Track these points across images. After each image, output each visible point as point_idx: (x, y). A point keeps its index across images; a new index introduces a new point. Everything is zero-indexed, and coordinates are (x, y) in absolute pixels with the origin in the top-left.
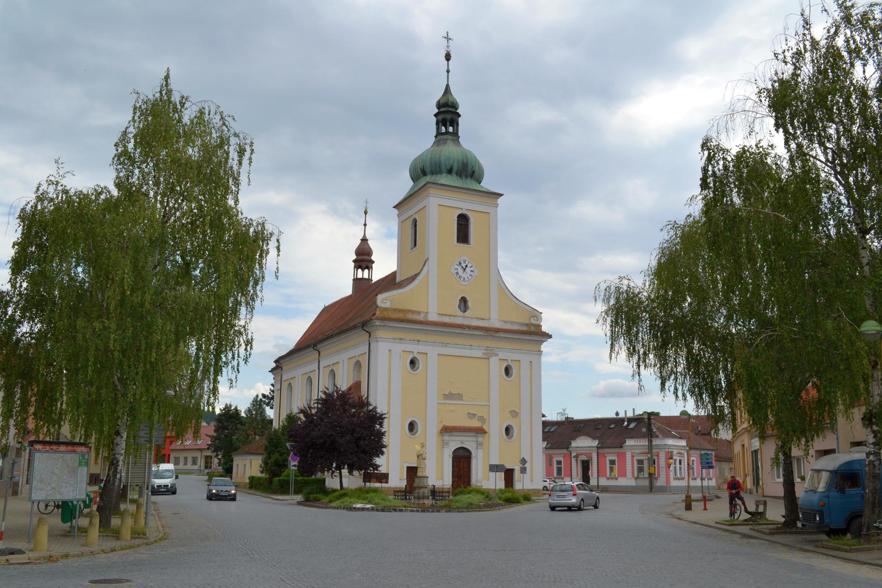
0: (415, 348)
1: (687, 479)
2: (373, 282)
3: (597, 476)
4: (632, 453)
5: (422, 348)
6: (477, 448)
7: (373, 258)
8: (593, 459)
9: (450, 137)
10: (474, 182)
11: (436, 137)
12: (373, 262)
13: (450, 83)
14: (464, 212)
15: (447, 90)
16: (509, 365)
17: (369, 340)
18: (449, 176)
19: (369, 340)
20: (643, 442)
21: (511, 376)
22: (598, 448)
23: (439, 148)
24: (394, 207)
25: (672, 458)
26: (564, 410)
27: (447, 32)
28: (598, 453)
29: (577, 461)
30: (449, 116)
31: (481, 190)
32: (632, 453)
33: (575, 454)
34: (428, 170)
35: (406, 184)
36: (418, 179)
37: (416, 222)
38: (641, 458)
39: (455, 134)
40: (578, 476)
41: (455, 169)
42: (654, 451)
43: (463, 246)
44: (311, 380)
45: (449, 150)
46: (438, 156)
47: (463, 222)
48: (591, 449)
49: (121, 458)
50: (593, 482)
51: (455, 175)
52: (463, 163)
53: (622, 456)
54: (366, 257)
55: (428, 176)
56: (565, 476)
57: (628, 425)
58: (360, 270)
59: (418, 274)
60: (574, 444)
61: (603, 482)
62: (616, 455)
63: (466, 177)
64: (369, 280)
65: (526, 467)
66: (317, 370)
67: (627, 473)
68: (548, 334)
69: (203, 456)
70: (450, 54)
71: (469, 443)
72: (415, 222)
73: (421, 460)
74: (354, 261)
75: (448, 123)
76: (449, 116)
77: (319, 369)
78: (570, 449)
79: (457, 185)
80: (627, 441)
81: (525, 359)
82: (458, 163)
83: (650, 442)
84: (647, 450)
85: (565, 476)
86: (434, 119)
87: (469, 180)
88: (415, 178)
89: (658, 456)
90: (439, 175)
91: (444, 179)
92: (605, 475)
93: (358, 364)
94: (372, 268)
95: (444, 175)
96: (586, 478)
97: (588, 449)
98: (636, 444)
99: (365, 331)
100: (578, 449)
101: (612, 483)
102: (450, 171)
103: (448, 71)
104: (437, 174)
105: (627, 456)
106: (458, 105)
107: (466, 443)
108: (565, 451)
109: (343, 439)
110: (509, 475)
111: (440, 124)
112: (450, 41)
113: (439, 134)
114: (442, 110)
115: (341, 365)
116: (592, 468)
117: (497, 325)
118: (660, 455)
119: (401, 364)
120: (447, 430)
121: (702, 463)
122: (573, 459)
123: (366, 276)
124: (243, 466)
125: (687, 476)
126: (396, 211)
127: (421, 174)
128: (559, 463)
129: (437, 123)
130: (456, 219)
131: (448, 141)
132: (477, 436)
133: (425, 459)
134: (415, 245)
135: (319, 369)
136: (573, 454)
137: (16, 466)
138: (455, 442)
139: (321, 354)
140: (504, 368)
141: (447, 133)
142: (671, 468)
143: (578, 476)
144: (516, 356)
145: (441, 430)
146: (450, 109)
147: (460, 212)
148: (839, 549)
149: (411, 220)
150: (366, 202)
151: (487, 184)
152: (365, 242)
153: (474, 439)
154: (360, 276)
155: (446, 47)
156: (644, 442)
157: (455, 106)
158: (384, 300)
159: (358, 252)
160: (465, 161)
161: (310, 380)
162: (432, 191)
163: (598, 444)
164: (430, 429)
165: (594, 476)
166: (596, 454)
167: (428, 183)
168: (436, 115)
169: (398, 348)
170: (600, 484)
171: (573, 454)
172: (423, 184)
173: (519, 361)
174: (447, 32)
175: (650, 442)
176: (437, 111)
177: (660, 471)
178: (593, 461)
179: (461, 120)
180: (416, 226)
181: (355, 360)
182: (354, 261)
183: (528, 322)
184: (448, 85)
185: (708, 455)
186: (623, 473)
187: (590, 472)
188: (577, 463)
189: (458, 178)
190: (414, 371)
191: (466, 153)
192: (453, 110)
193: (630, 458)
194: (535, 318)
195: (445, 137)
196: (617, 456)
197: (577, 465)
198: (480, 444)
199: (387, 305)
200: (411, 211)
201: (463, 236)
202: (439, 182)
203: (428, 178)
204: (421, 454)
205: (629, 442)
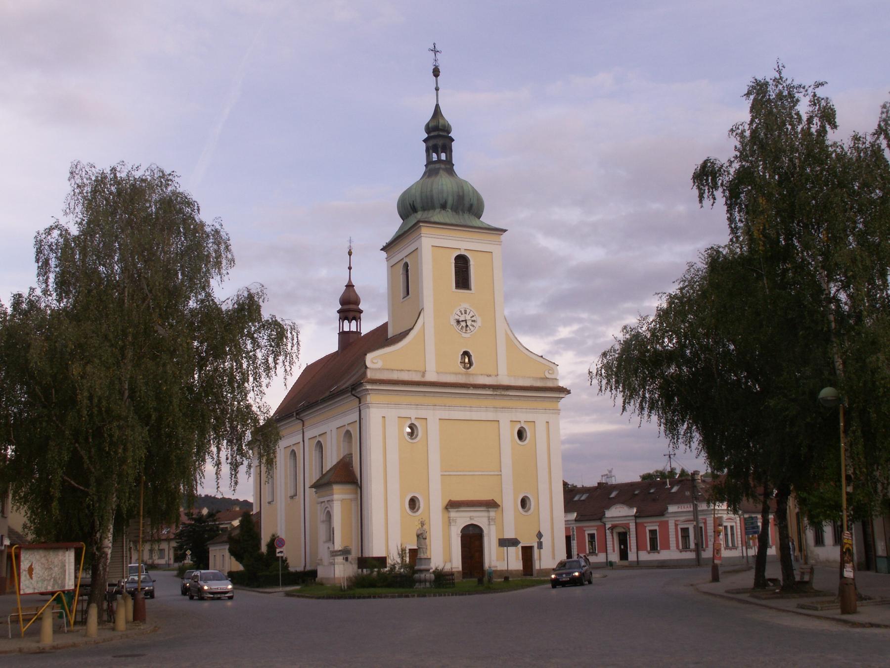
0: (413, 414)
1: (741, 548)
2: (362, 335)
4: (676, 521)
5: (422, 413)
6: (489, 525)
7: (361, 307)
8: (631, 530)
9: (443, 166)
10: (472, 218)
12: (361, 312)
14: (463, 253)
15: (437, 112)
16: (522, 427)
17: (359, 407)
18: (443, 212)
19: (359, 407)
20: (687, 507)
21: (525, 440)
23: (430, 180)
24: (381, 250)
25: (721, 525)
26: (610, 472)
27: (434, 44)
28: (636, 523)
29: (612, 533)
30: (440, 142)
31: (480, 225)
32: (676, 521)
33: (610, 526)
34: (418, 205)
35: (395, 224)
37: (408, 266)
38: (686, 526)
39: (449, 163)
40: (614, 551)
42: (700, 517)
44: (295, 453)
45: (443, 183)
46: (429, 189)
47: (462, 264)
48: (628, 518)
49: (109, 551)
50: (632, 556)
51: (450, 210)
53: (664, 526)
54: (352, 307)
56: (599, 552)
57: (672, 488)
58: (346, 322)
60: (609, 513)
61: (644, 556)
64: (358, 333)
66: (302, 443)
67: (671, 545)
68: (566, 389)
69: (171, 548)
70: (439, 69)
71: (479, 518)
72: (406, 265)
73: (422, 540)
74: (339, 312)
75: (440, 150)
76: (440, 142)
77: (303, 441)
78: (604, 520)
79: (453, 222)
81: (540, 419)
83: (695, 507)
84: (692, 517)
85: (599, 552)
87: (466, 216)
89: (705, 523)
90: (431, 212)
91: (438, 216)
92: (646, 549)
93: (348, 434)
94: (360, 318)
95: (438, 210)
96: (624, 555)
97: (623, 519)
98: (680, 510)
99: (354, 395)
101: (654, 557)
102: (444, 206)
104: (429, 210)
105: (670, 524)
106: (450, 127)
107: (475, 519)
108: (598, 523)
109: (174, 458)
110: (527, 553)
111: (431, 151)
113: (429, 162)
114: (432, 134)
115: (328, 435)
117: (505, 381)
118: (708, 522)
119: (397, 432)
120: (452, 505)
121: (746, 529)
122: (607, 531)
123: (354, 329)
125: (740, 545)
126: (384, 255)
128: (592, 536)
129: (427, 150)
131: (441, 172)
132: (488, 511)
133: (426, 539)
135: (303, 441)
136: (608, 526)
138: (463, 518)
139: (305, 423)
140: (420, 499)
141: (439, 161)
142: (721, 537)
143: (614, 551)
144: (530, 417)
145: (447, 505)
146: (441, 133)
148: (809, 608)
149: (402, 264)
150: (350, 241)
151: (487, 218)
152: (351, 288)
153: (486, 514)
154: (346, 329)
156: (688, 508)
157: (447, 129)
158: (375, 361)
159: (345, 301)
160: (461, 194)
161: (293, 453)
163: (636, 513)
164: (434, 505)
166: (634, 524)
167: (419, 222)
168: (425, 141)
169: (392, 414)
170: (609, 560)
173: (534, 422)
174: (434, 44)
176: (426, 136)
177: (709, 540)
179: (454, 145)
180: (407, 271)
181: (344, 430)
182: (339, 312)
183: (543, 376)
184: (437, 106)
185: (752, 518)
186: (667, 547)
188: (612, 535)
189: (454, 213)
190: (412, 439)
191: (462, 184)
193: (674, 527)
194: (550, 372)
195: (437, 166)
196: (659, 526)
197: (613, 538)
198: (492, 519)
199: (379, 364)
200: (401, 254)
201: (463, 279)
202: (432, 220)
203: (419, 215)
204: (422, 534)
205: (672, 509)
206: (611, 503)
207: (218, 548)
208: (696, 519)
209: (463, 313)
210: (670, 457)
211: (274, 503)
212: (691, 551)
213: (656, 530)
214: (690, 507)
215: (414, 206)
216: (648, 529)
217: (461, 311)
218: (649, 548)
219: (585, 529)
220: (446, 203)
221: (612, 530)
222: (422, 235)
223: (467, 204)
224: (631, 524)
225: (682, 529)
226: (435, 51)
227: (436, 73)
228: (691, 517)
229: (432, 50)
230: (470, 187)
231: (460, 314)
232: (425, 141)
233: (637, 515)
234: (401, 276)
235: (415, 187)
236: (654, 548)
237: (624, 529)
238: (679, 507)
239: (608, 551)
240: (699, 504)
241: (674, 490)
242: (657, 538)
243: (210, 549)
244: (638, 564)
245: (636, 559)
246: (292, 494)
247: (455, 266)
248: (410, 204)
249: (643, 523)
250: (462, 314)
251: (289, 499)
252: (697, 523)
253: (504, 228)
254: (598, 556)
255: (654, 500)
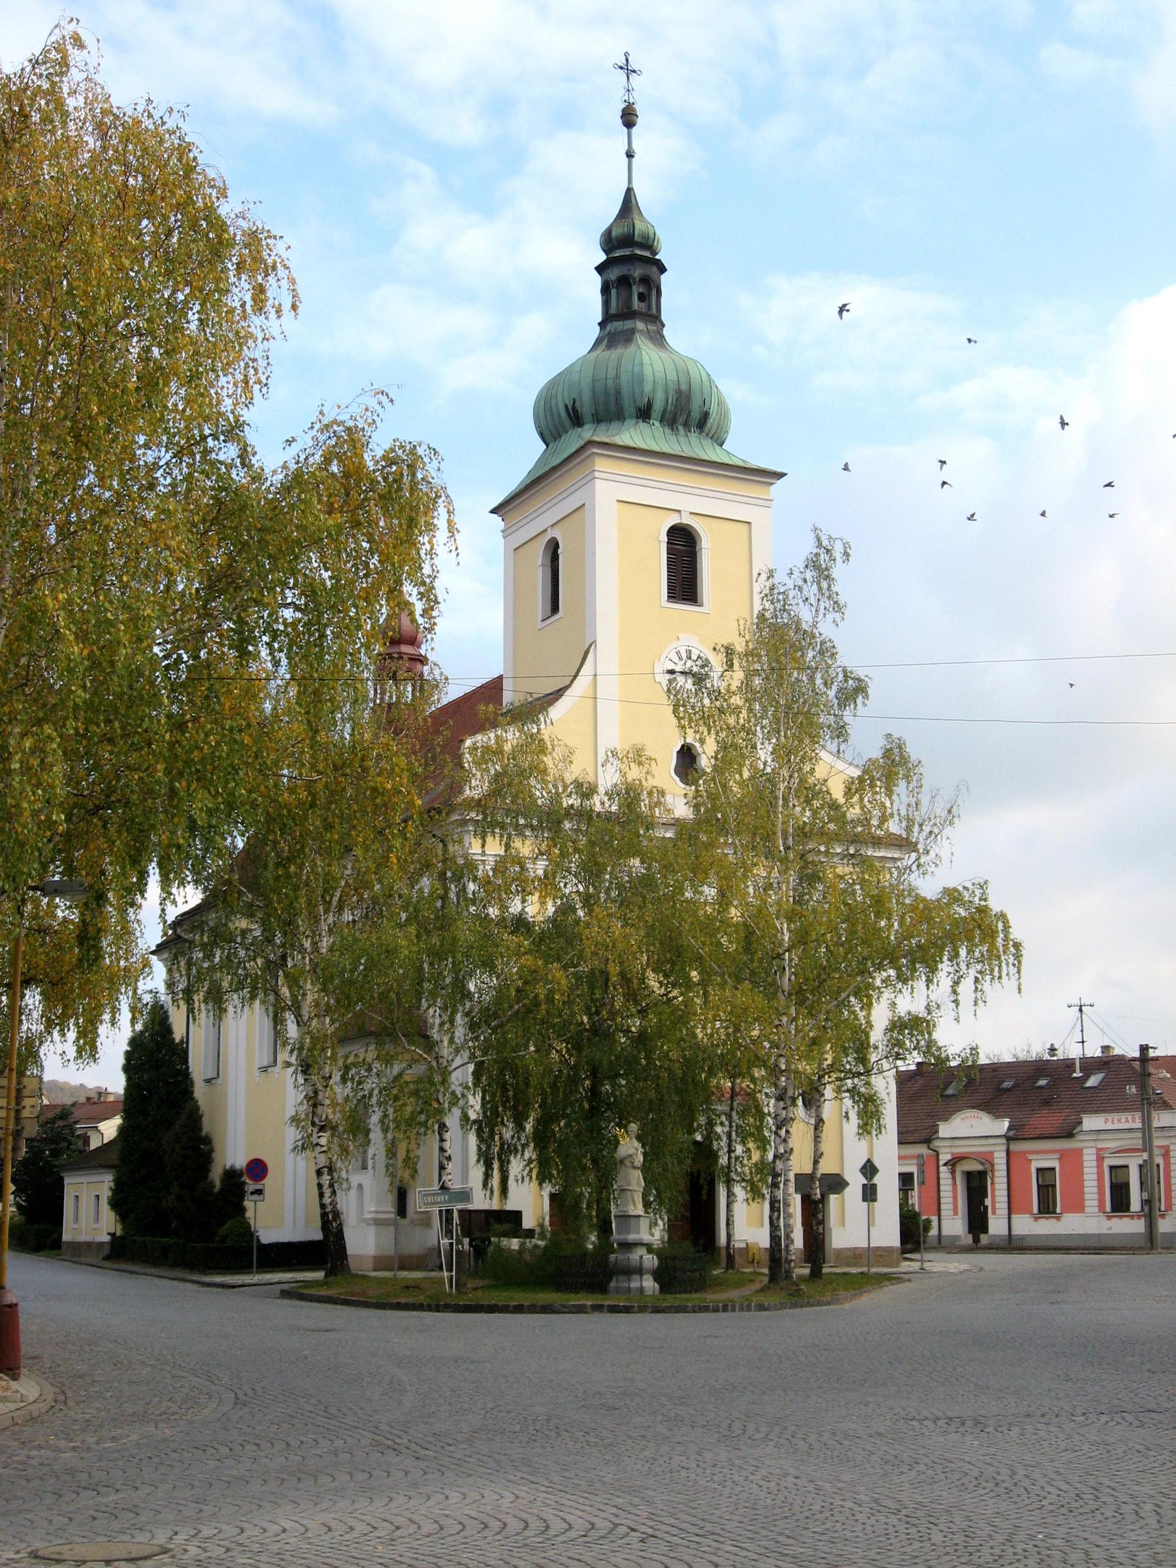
3: (1006, 1212)
4: (1099, 1150)
8: (996, 1167)
9: (640, 325)
10: (707, 442)
11: (602, 325)
13: (635, 186)
14: (686, 520)
15: (628, 205)
18: (642, 424)
20: (1127, 1121)
22: (1009, 1139)
23: (615, 353)
24: (493, 511)
27: (626, 55)
29: (953, 1172)
31: (726, 460)
32: (1099, 1150)
33: (949, 1157)
34: (586, 410)
36: (560, 436)
37: (557, 546)
41: (658, 406)
42: (1157, 1142)
43: (683, 609)
46: (610, 383)
50: (997, 1226)
51: (657, 424)
52: (679, 392)
53: (1073, 1159)
55: (586, 427)
57: (1086, 1077)
59: (558, 694)
61: (1026, 1225)
62: (1057, 1156)
63: (686, 425)
65: (875, 1186)
67: (1087, 1203)
72: (553, 548)
78: (936, 1143)
79: (666, 449)
80: (1084, 1120)
82: (666, 393)
83: (1147, 1121)
84: (1141, 1141)
86: (597, 280)
87: (693, 436)
88: (550, 432)
90: (615, 425)
91: (632, 435)
95: (629, 422)
96: (977, 1221)
97: (984, 1142)
98: (1109, 1126)
100: (956, 1143)
101: (1046, 1227)
102: (644, 414)
103: (630, 155)
108: (922, 1150)
112: (633, 76)
114: (618, 254)
116: (993, 1190)
122: (943, 1169)
124: (93, 1199)
127: (567, 422)
130: (664, 538)
134: (555, 608)
136: (944, 1158)
137: (41, 1553)
143: (956, 1213)
146: (638, 252)
147: (674, 520)
155: (623, 91)
156: (1133, 1120)
160: (684, 387)
162: (603, 466)
163: (1009, 1129)
165: (998, 1212)
166: (1004, 1154)
168: (600, 269)
170: (1014, 1233)
171: (944, 1158)
172: (573, 450)
174: (626, 55)
175: (1147, 1121)
178: (997, 1174)
184: (629, 191)
187: (988, 1202)
188: (954, 1178)
189: (667, 431)
191: (683, 367)
192: (647, 254)
193: (1095, 1164)
197: (954, 1184)
203: (587, 432)
204: (630, 1156)
205: (1091, 1122)
206: (948, 1108)
207: (84, 1179)
208: (1147, 1146)
209: (684, 656)
210: (1081, 1010)
211: (220, 1081)
212: (1132, 1217)
213: (912, 1174)
214: (1133, 1121)
215: (574, 408)
216: (1034, 1165)
217: (678, 653)
218: (1035, 1210)
219: (1030, 1157)
220: (650, 405)
221: (954, 1165)
222: (597, 474)
223: (696, 414)
224: (996, 1155)
225: (1112, 1168)
226: (627, 69)
227: (629, 118)
228: (1138, 1143)
229: (621, 68)
230: (703, 373)
231: (676, 659)
232: (600, 269)
233: (1011, 1133)
234: (540, 570)
235: (579, 363)
236: (1047, 1208)
237: (982, 1163)
238: (1106, 1121)
239: (943, 1213)
240: (1154, 1114)
241: (1092, 1082)
242: (1054, 1186)
243: (67, 1181)
244: (1012, 1245)
245: (1006, 1232)
246: (265, 1063)
247: (668, 549)
248: (566, 406)
249: (1025, 1153)
250: (681, 659)
251: (257, 1073)
252: (1151, 1156)
253: (779, 470)
254: (1063, 1219)
255: (1047, 1103)
